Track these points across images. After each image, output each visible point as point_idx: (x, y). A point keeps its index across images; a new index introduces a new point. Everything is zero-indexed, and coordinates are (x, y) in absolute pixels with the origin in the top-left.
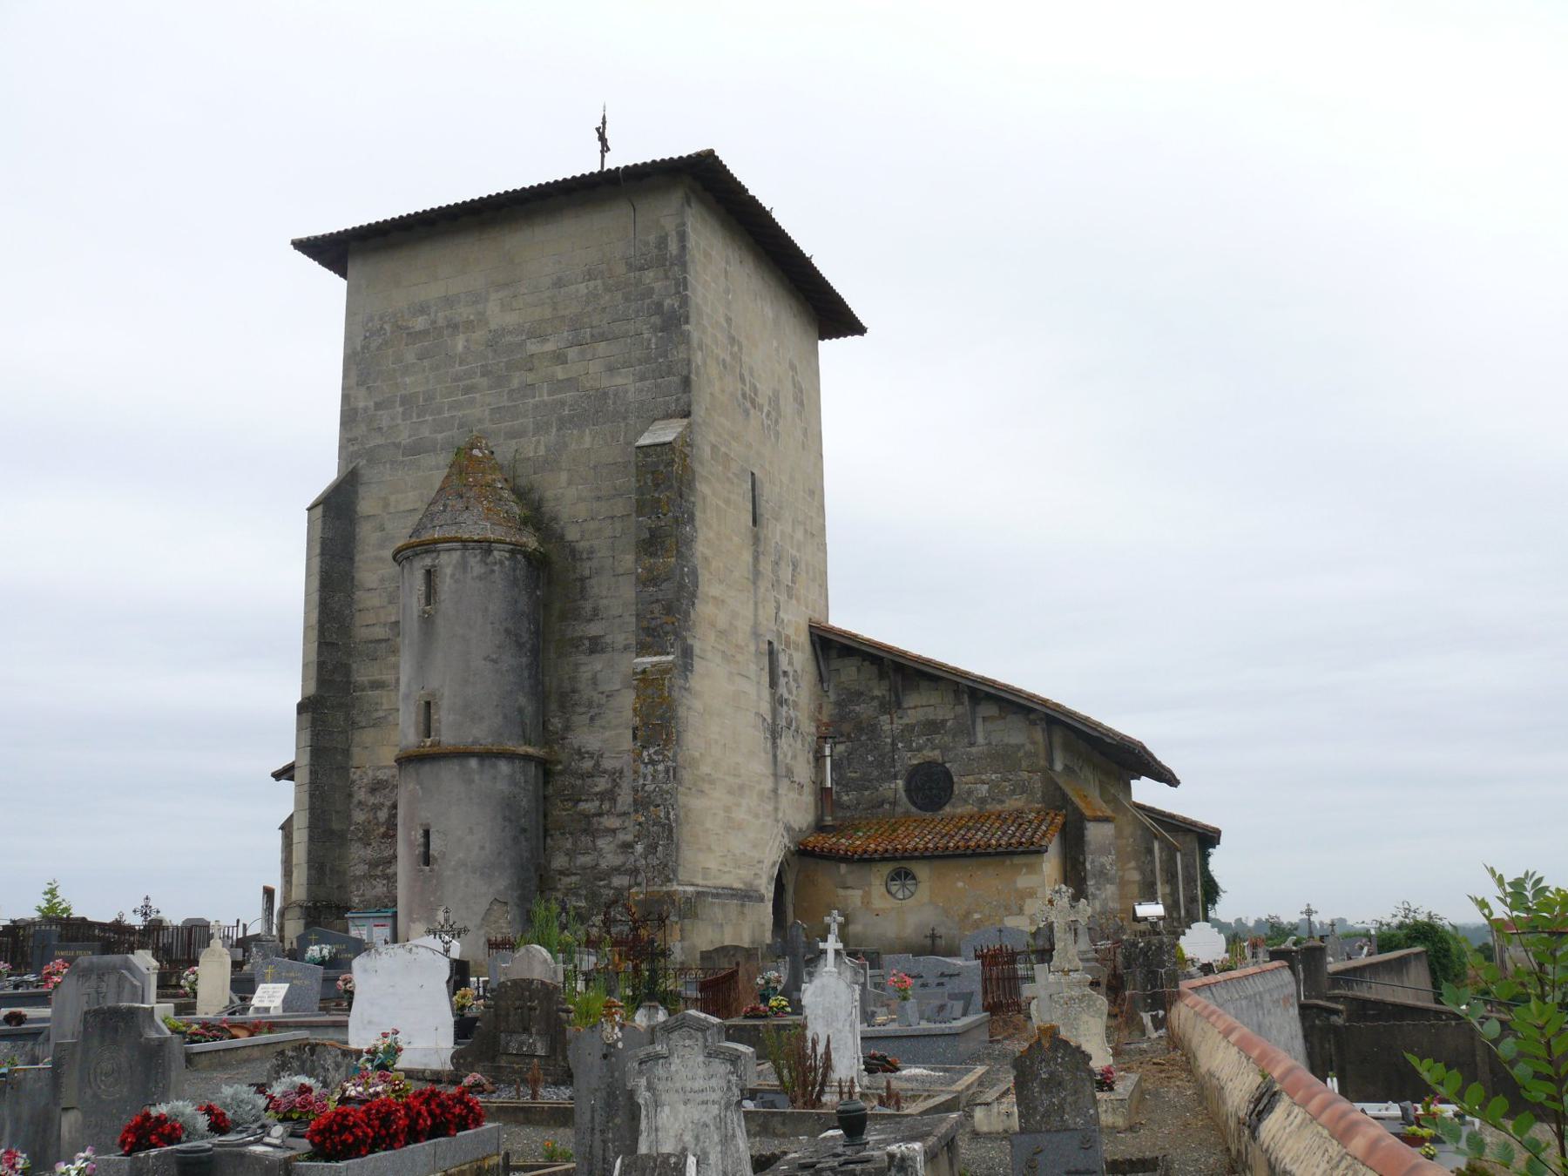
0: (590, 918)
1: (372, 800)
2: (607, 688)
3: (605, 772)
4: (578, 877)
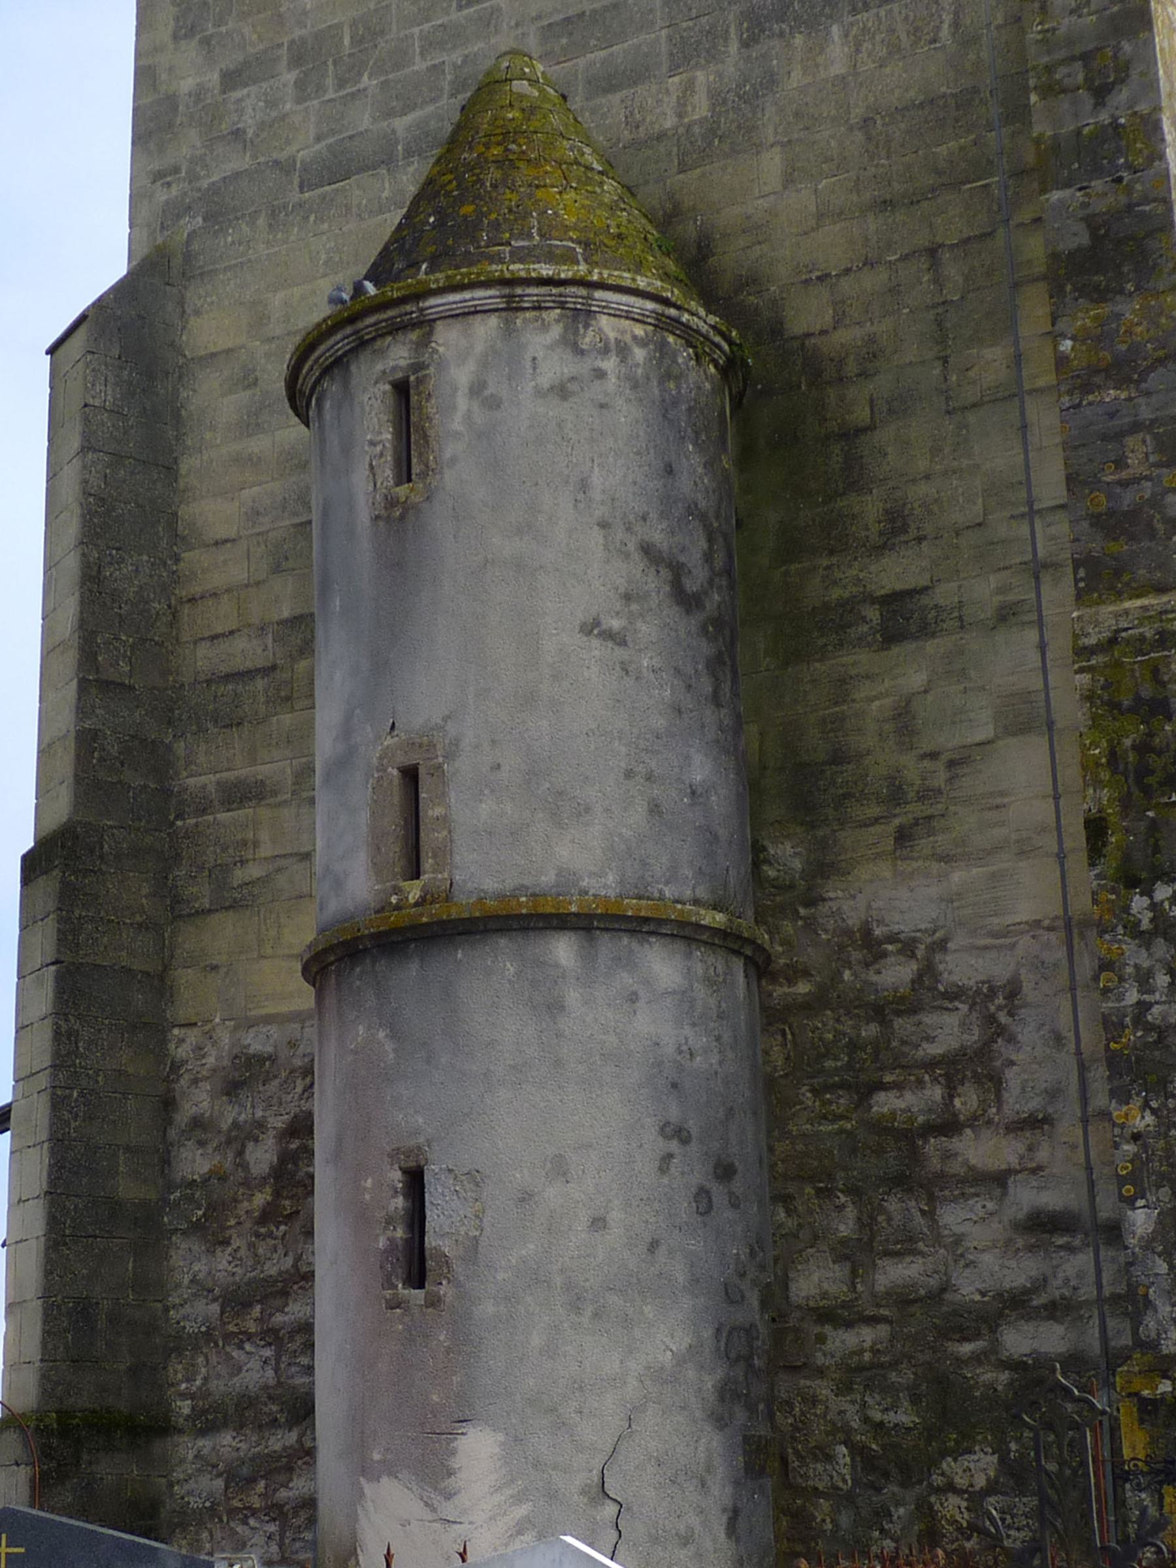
0: (934, 1463)
1: (229, 1115)
2: (949, 740)
3: (956, 994)
4: (883, 1330)
